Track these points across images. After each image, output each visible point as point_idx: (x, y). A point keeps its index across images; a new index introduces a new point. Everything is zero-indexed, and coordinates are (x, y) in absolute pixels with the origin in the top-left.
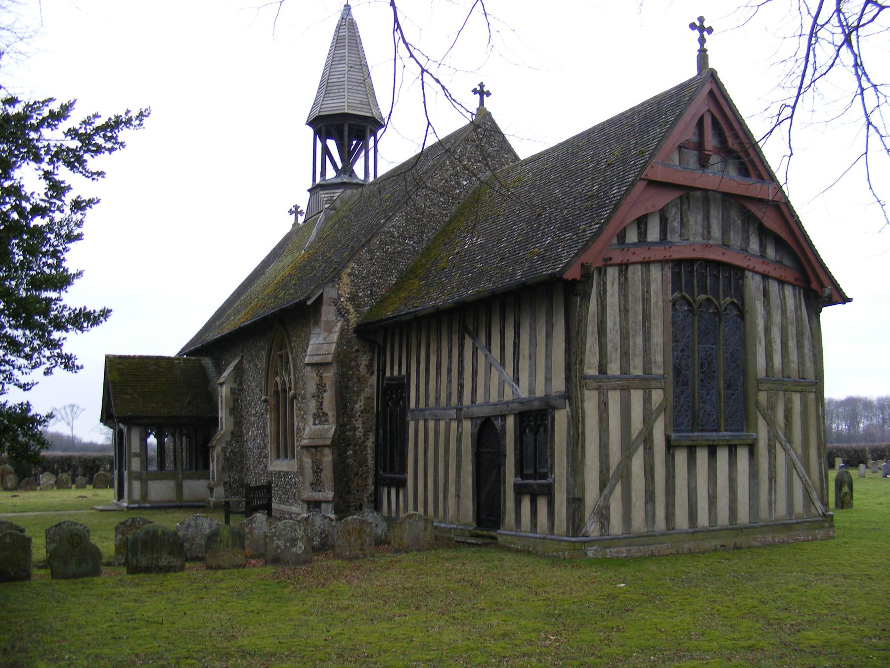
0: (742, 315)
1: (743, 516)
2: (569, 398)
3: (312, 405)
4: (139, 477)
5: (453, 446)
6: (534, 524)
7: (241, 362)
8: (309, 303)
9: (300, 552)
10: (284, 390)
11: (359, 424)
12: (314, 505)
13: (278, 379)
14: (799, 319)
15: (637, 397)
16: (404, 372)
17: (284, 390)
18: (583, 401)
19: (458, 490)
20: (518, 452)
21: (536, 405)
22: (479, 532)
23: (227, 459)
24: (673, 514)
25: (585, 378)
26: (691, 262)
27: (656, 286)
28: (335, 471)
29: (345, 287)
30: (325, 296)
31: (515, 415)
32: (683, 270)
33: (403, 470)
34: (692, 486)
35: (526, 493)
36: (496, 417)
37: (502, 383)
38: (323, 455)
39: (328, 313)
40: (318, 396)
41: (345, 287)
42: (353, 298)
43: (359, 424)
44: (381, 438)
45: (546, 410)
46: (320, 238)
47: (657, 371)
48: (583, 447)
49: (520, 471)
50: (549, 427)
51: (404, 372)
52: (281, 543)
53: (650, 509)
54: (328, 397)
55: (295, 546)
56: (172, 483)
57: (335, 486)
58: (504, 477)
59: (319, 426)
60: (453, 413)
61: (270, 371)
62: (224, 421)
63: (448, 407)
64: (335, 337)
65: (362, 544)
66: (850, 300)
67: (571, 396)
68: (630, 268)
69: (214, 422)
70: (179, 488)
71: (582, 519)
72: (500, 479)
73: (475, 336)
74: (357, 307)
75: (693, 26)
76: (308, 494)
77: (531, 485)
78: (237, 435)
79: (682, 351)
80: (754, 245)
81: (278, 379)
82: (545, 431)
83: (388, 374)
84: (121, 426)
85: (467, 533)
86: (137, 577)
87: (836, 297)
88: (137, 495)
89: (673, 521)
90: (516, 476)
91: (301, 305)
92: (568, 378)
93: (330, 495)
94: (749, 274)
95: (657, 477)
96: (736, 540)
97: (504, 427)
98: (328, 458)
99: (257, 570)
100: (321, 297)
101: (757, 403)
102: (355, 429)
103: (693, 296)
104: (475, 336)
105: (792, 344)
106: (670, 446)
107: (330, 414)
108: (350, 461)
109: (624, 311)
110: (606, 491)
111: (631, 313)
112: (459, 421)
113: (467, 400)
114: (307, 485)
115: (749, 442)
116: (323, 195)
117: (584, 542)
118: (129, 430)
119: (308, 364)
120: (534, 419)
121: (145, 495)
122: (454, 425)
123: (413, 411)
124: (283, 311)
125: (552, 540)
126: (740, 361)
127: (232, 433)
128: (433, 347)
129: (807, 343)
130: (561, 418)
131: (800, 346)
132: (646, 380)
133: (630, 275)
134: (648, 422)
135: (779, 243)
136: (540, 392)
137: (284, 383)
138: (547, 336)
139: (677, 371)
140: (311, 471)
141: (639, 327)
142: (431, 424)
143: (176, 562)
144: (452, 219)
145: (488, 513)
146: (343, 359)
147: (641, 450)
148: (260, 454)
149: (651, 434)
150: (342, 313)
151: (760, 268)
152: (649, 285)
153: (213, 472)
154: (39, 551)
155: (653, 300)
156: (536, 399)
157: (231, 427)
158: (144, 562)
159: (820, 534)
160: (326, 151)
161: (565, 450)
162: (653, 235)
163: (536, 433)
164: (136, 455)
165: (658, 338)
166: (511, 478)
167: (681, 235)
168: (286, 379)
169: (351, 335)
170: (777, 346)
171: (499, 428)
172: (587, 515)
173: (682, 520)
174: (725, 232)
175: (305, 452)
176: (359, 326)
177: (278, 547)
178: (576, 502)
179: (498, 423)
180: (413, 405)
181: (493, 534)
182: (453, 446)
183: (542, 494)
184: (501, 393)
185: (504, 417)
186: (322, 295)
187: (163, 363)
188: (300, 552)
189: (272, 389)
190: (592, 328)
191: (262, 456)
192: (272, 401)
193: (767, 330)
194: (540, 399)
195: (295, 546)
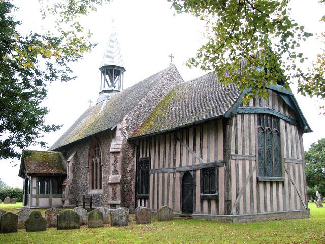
0: (279, 135)
1: (282, 210)
2: (225, 162)
3: (112, 168)
4: (35, 197)
5: (171, 182)
6: (209, 211)
7: (76, 153)
8: (112, 129)
9: (124, 221)
10: (97, 164)
11: (129, 176)
12: (113, 206)
13: (94, 159)
14: (296, 137)
15: (247, 163)
16: (148, 156)
17: (97, 164)
18: (230, 164)
19: (173, 199)
20: (202, 184)
21: (210, 166)
22: (184, 215)
23: (70, 190)
24: (259, 207)
25: (231, 155)
26: (263, 114)
27: (252, 123)
28: (121, 193)
29: (124, 124)
30: (117, 127)
31: (201, 170)
32: (262, 117)
33: (147, 192)
34: (265, 196)
35: (206, 199)
36: (192, 171)
37: (194, 158)
38: (117, 187)
39: (118, 133)
40: (115, 164)
41: (124, 124)
42: (127, 128)
43: (129, 176)
44: (137, 181)
45: (215, 167)
46: (106, 108)
47: (254, 153)
48: (231, 181)
49: (203, 190)
50: (216, 174)
51: (148, 156)
52: (117, 217)
53: (252, 205)
54: (119, 165)
55: (122, 219)
56: (48, 199)
57: (121, 199)
58: (195, 193)
59: (115, 176)
60: (171, 170)
61: (91, 156)
62: (69, 175)
63: (169, 168)
64: (121, 142)
65: (147, 218)
66: (312, 131)
67: (226, 162)
68: (245, 116)
69: (64, 176)
70: (50, 201)
71: (230, 208)
72: (193, 194)
73: (181, 141)
74: (129, 132)
75: (169, 56)
76: (111, 202)
77: (208, 196)
78: (74, 181)
79: (261, 147)
80: (282, 110)
81: (94, 159)
82: (214, 176)
83: (141, 157)
84: (28, 177)
85: (178, 215)
86: (60, 231)
87: (309, 130)
88: (34, 204)
89: (259, 210)
90: (201, 192)
91: (109, 130)
92: (225, 155)
93: (119, 202)
94: (281, 120)
95: (254, 193)
96: (280, 216)
97: (195, 175)
98: (119, 188)
99: (107, 228)
100: (116, 127)
101: (284, 167)
102: (128, 177)
103: (264, 127)
104: (181, 141)
105: (294, 146)
106: (258, 182)
107: (119, 171)
108: (125, 189)
109: (243, 131)
110: (238, 198)
111: (245, 132)
112: (174, 173)
113: (178, 165)
114: (110, 198)
115: (283, 181)
116: (105, 94)
117: (232, 217)
118: (32, 178)
119: (111, 152)
120: (209, 172)
121: (37, 204)
122: (172, 175)
123: (152, 170)
124: (100, 133)
125: (218, 216)
126: (279, 152)
127: (72, 180)
128: (162, 146)
129: (299, 146)
130: (222, 171)
131: (297, 147)
132: (250, 156)
133: (244, 118)
134: (250, 171)
135: (290, 110)
136: (212, 160)
137: (97, 160)
138: (215, 139)
139: (260, 154)
140: (112, 193)
141: (248, 137)
142: (161, 175)
143: (77, 225)
144: (162, 102)
145: (187, 209)
146: (124, 150)
147: (249, 183)
148: (85, 187)
149: (252, 177)
150: (123, 134)
151: (284, 118)
152: (250, 122)
153: (64, 195)
154: (202, 194)
155: (252, 127)
156: (210, 163)
157: (72, 178)
158: (64, 225)
159: (306, 215)
160: (105, 80)
161: (224, 183)
162: (251, 104)
163: (210, 176)
164: (35, 188)
165: (253, 142)
166: (198, 193)
167: (260, 105)
168: (98, 159)
169: (126, 142)
170: (290, 147)
171: (193, 175)
172: (232, 206)
173: (262, 210)
174: (273, 105)
175: (110, 186)
176: (129, 139)
177: (116, 219)
178: (228, 202)
179: (192, 173)
180: (152, 168)
181: (190, 215)
182: (171, 182)
183: (213, 199)
184: (194, 162)
185: (195, 171)
186: (116, 127)
187: (45, 154)
188: (124, 221)
189: (91, 163)
190: (233, 137)
191: (86, 188)
192: (91, 168)
193: (287, 141)
194: (213, 163)
195: (122, 219)
